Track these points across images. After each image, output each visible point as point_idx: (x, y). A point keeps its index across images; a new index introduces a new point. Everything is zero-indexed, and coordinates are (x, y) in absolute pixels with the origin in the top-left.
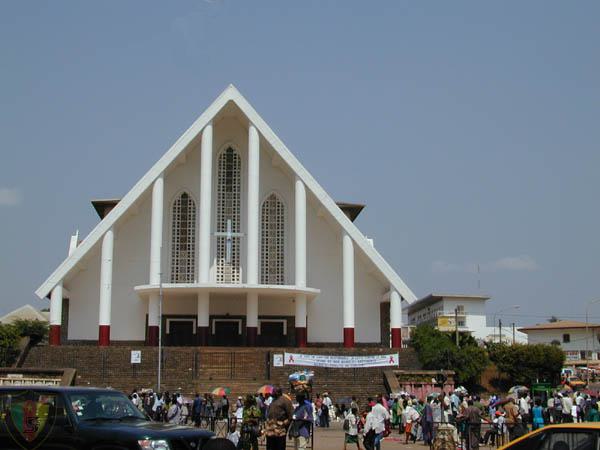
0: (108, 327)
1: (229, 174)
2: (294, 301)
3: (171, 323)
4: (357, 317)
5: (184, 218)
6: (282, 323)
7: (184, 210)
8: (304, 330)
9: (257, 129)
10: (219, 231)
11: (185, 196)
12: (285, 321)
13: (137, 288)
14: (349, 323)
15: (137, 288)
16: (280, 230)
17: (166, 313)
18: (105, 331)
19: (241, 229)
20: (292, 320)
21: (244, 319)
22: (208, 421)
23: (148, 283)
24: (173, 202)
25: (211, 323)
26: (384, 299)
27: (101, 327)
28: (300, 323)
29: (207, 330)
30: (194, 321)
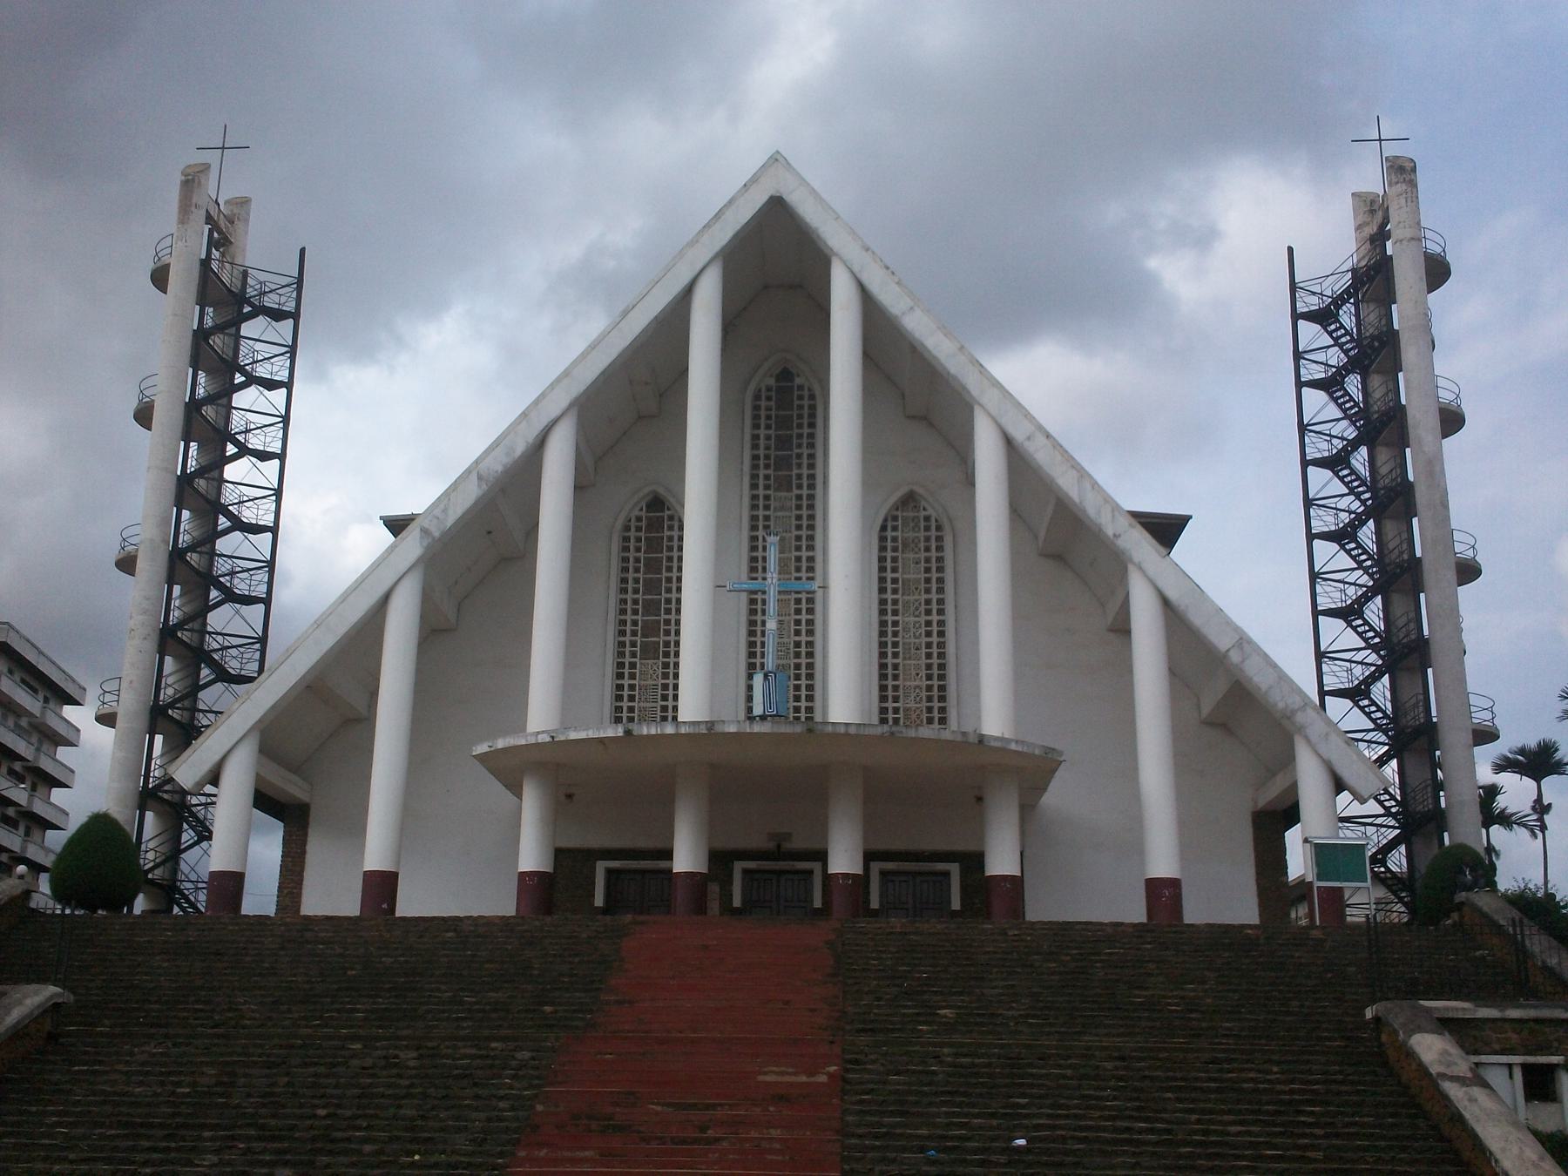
0: (1174, 884)
1: (784, 442)
2: (980, 799)
3: (609, 872)
4: (1187, 846)
6: (947, 874)
7: (654, 545)
8: (1014, 886)
9: (989, 414)
12: (954, 869)
14: (1163, 864)
15: (482, 748)
16: (761, 513)
17: (722, 844)
18: (1163, 894)
20: (974, 861)
21: (822, 856)
22: (1239, 1000)
23: (521, 727)
24: (619, 524)
25: (866, 868)
26: (1270, 794)
27: (369, 876)
28: (1002, 861)
29: (859, 883)
30: (816, 867)
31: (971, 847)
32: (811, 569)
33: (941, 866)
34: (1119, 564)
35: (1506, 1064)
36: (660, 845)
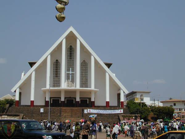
0: (33, 101)
1: (71, 54)
2: (91, 93)
3: (53, 100)
4: (110, 98)
5: (57, 67)
6: (87, 100)
7: (57, 65)
8: (94, 102)
10: (67, 71)
11: (57, 60)
12: (88, 99)
13: (42, 89)
14: (108, 100)
17: (51, 97)
18: (32, 102)
19: (74, 71)
20: (90, 99)
21: (75, 98)
23: (46, 87)
24: (53, 62)
25: (65, 100)
26: (119, 92)
27: (31, 101)
28: (93, 100)
29: (64, 102)
30: (60, 99)
31: (75, 97)
32: (74, 70)
33: (72, 99)
34: (105, 72)
35: (183, 101)
36: (59, 97)
